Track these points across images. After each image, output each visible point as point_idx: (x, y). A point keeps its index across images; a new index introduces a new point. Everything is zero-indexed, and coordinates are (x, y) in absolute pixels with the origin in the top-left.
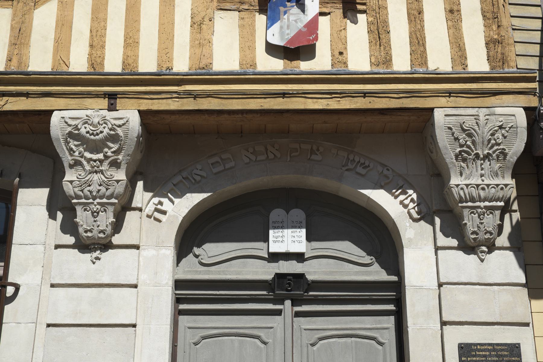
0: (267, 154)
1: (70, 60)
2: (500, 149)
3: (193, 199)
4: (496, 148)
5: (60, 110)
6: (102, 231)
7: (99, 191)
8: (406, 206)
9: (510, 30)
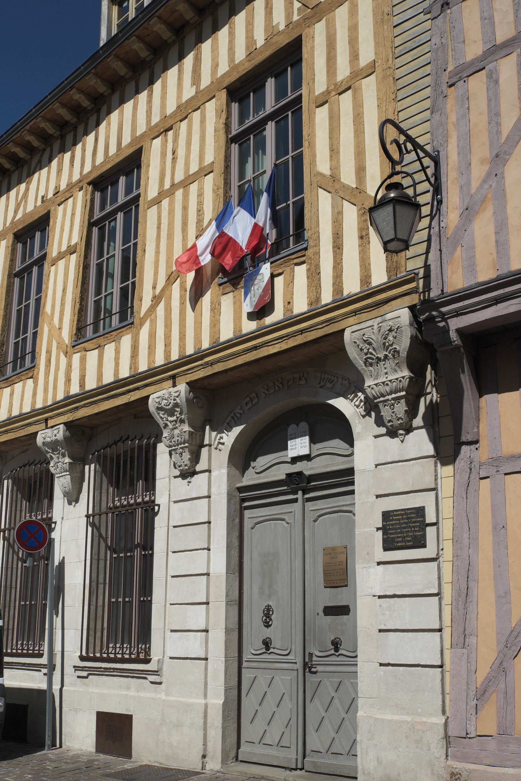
3: (237, 430)
4: (390, 348)
6: (186, 465)
8: (358, 406)
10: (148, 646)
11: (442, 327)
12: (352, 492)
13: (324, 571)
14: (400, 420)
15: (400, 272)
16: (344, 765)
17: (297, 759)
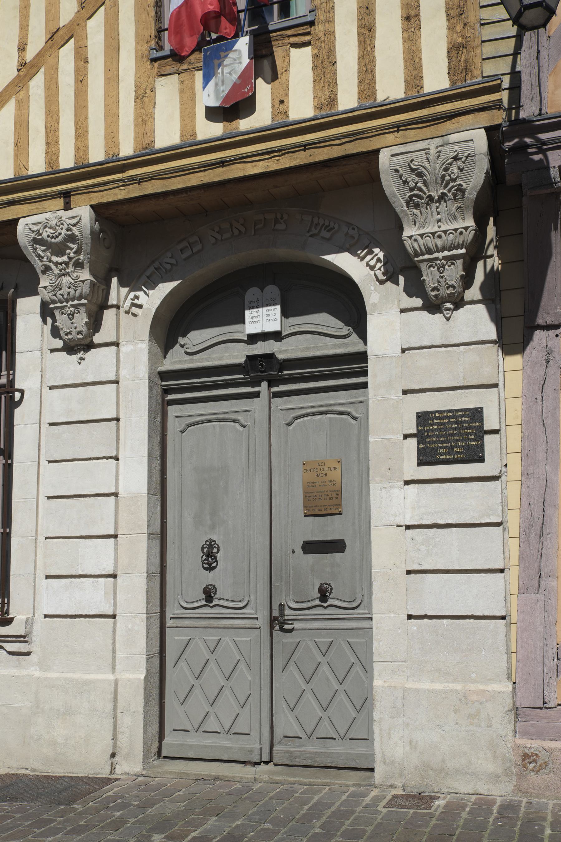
0: (232, 231)
1: (29, 163)
2: (456, 186)
4: (451, 184)
5: (25, 217)
6: (79, 333)
7: (69, 293)
8: (372, 268)
9: (478, 26)
10: (6, 600)
11: (537, 161)
12: (365, 385)
13: (304, 493)
14: (451, 289)
15: (472, 77)
16: (338, 753)
17: (261, 749)
